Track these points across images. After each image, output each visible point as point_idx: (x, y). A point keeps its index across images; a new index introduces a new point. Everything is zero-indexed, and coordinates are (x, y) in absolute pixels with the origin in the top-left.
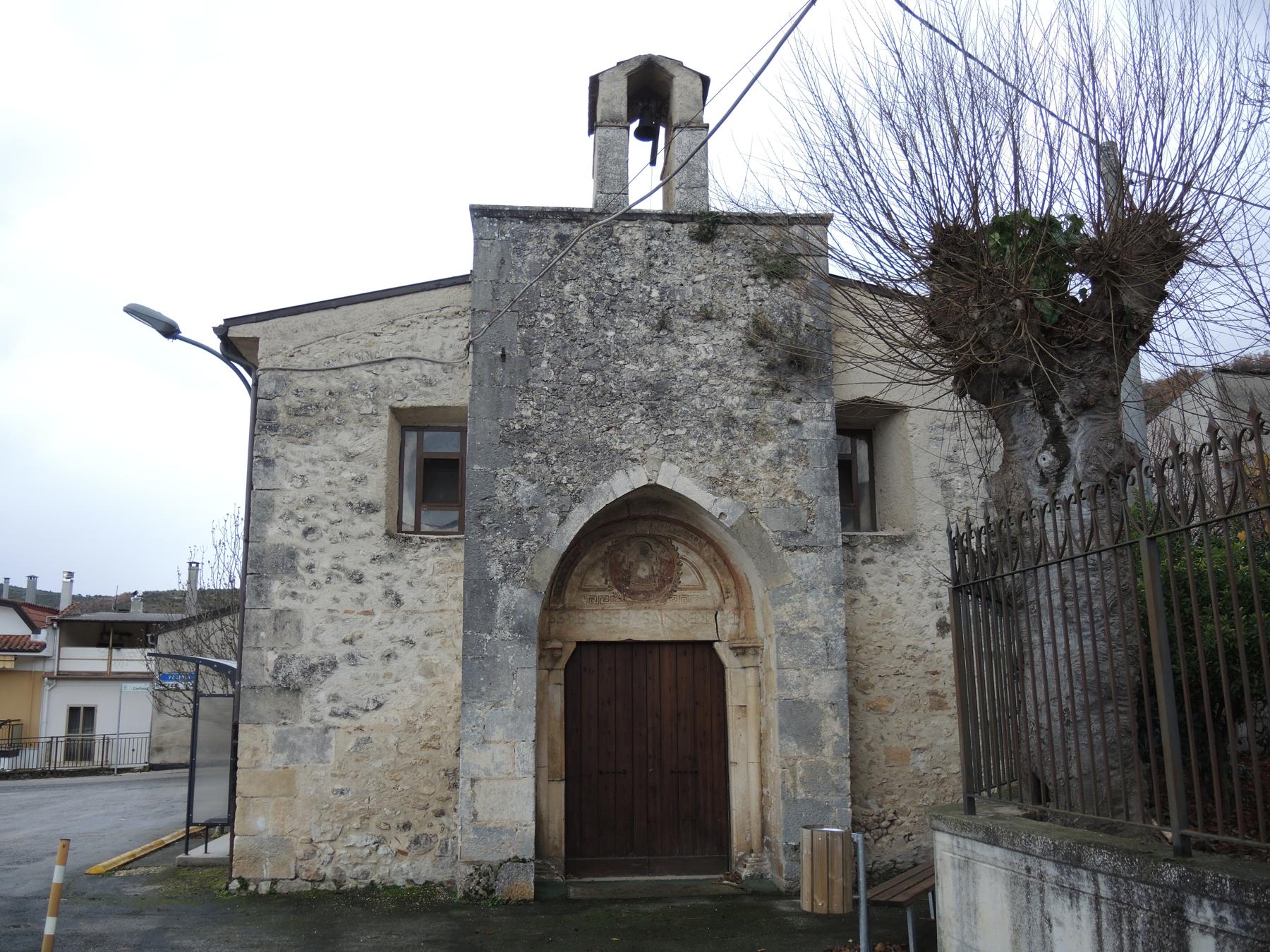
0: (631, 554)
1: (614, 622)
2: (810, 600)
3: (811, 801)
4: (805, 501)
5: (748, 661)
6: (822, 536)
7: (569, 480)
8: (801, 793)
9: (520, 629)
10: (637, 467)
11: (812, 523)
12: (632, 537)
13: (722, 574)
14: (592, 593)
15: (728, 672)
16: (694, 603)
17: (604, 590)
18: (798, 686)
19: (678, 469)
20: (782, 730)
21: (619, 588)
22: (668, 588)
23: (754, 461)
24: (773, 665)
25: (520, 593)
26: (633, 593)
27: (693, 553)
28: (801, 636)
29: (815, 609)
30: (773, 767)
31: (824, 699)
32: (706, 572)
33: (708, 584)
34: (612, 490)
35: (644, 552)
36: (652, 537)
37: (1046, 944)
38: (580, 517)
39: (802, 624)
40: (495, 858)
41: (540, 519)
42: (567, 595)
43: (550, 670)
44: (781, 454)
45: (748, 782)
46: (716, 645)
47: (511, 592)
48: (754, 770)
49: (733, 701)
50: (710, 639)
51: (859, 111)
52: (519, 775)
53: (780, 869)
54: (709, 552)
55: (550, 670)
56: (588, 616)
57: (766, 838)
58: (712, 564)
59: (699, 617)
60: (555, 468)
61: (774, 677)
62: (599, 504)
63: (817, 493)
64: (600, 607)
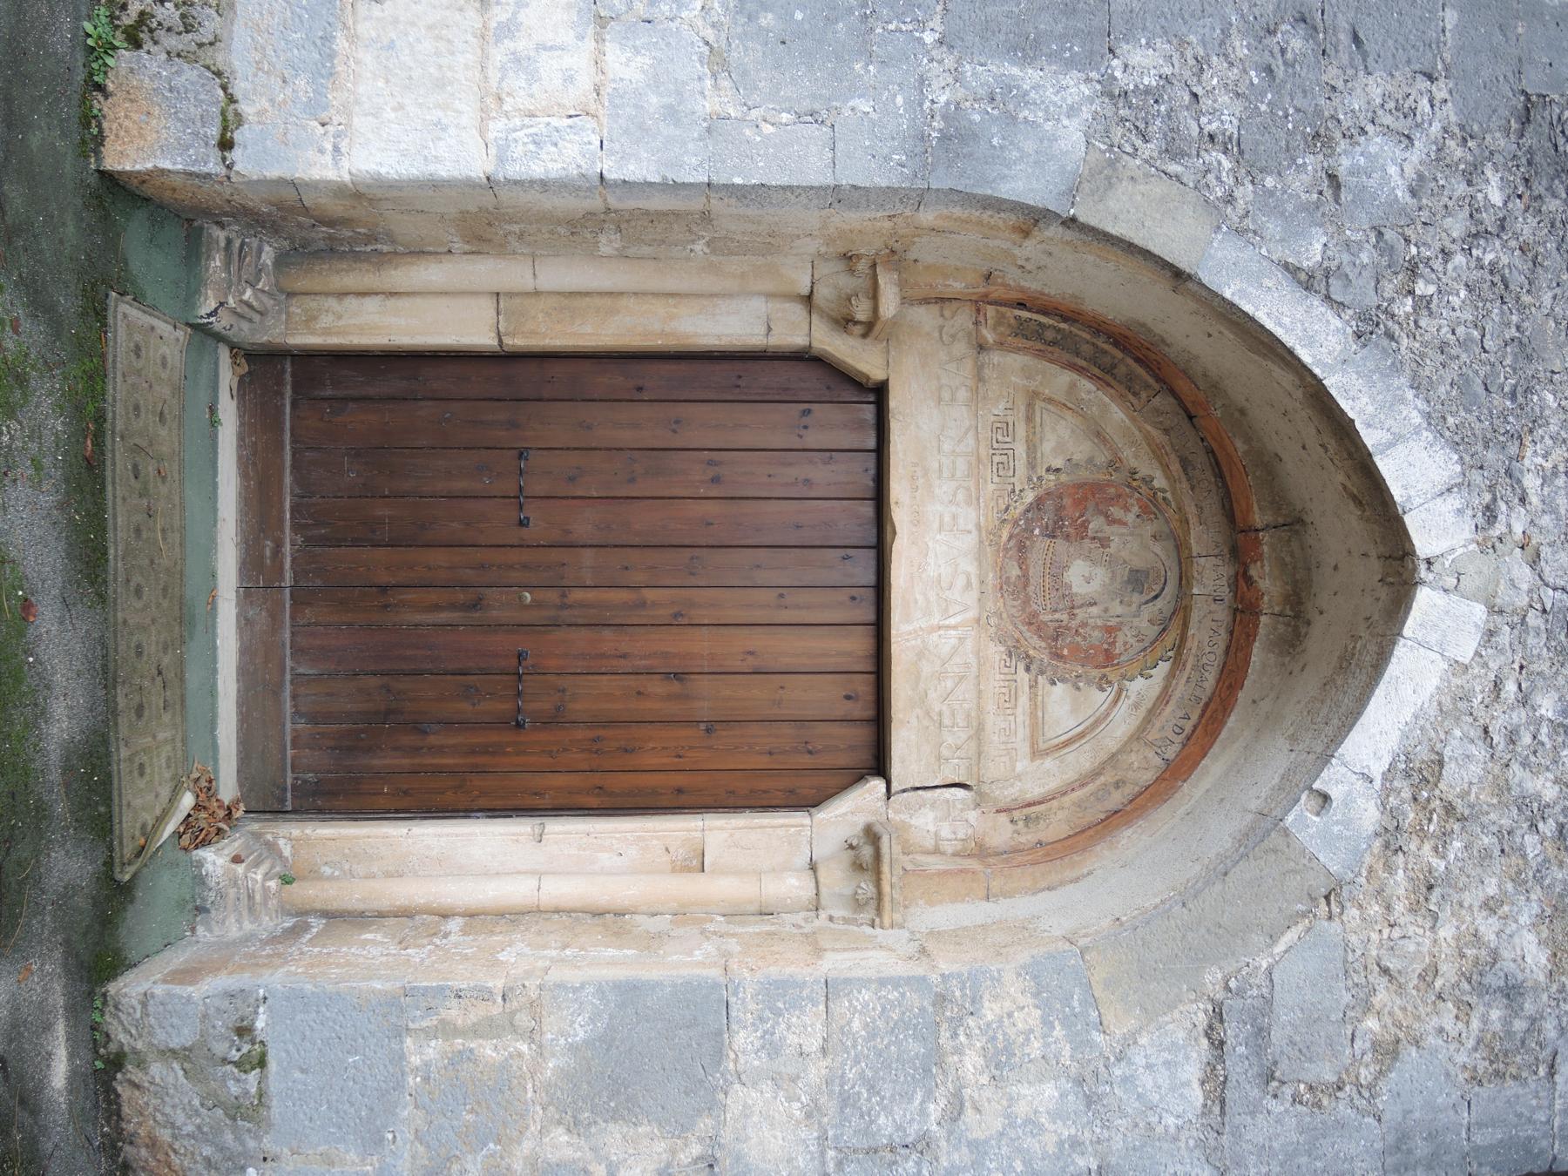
0: (1132, 540)
1: (944, 489)
2: (1050, 1090)
3: (399, 1086)
4: (1365, 1075)
5: (836, 879)
6: (1258, 1130)
7: (1423, 304)
8: (423, 1053)
9: (956, 136)
10: (1467, 531)
11: (1296, 1099)
13: (1079, 804)
14: (1021, 430)
15: (800, 818)
16: (993, 722)
17: (1032, 465)
18: (773, 1048)
19: (1465, 653)
20: (629, 991)
21: (1038, 504)
22: (1036, 646)
23: (1490, 906)
24: (835, 963)
25: (1071, 137)
26: (1022, 548)
28: (933, 1063)
29: (1022, 1109)
30: (518, 957)
31: (727, 1136)
32: (1081, 760)
33: (1049, 763)
34: (1397, 439)
35: (1137, 580)
36: (1182, 610)
38: (1315, 336)
39: (971, 1063)
40: (239, 56)
42: (1015, 361)
43: (808, 300)
44: (1512, 992)
45: (487, 874)
46: (878, 785)
47: (1072, 111)
48: (517, 891)
49: (718, 832)
50: (896, 769)
52: (496, 128)
53: (188, 975)
54: (1143, 767)
55: (808, 300)
56: (960, 415)
57: (317, 924)
58: (1107, 778)
60: (1459, 259)
61: (794, 966)
62: (1355, 397)
63: (1392, 1114)
64: (983, 452)
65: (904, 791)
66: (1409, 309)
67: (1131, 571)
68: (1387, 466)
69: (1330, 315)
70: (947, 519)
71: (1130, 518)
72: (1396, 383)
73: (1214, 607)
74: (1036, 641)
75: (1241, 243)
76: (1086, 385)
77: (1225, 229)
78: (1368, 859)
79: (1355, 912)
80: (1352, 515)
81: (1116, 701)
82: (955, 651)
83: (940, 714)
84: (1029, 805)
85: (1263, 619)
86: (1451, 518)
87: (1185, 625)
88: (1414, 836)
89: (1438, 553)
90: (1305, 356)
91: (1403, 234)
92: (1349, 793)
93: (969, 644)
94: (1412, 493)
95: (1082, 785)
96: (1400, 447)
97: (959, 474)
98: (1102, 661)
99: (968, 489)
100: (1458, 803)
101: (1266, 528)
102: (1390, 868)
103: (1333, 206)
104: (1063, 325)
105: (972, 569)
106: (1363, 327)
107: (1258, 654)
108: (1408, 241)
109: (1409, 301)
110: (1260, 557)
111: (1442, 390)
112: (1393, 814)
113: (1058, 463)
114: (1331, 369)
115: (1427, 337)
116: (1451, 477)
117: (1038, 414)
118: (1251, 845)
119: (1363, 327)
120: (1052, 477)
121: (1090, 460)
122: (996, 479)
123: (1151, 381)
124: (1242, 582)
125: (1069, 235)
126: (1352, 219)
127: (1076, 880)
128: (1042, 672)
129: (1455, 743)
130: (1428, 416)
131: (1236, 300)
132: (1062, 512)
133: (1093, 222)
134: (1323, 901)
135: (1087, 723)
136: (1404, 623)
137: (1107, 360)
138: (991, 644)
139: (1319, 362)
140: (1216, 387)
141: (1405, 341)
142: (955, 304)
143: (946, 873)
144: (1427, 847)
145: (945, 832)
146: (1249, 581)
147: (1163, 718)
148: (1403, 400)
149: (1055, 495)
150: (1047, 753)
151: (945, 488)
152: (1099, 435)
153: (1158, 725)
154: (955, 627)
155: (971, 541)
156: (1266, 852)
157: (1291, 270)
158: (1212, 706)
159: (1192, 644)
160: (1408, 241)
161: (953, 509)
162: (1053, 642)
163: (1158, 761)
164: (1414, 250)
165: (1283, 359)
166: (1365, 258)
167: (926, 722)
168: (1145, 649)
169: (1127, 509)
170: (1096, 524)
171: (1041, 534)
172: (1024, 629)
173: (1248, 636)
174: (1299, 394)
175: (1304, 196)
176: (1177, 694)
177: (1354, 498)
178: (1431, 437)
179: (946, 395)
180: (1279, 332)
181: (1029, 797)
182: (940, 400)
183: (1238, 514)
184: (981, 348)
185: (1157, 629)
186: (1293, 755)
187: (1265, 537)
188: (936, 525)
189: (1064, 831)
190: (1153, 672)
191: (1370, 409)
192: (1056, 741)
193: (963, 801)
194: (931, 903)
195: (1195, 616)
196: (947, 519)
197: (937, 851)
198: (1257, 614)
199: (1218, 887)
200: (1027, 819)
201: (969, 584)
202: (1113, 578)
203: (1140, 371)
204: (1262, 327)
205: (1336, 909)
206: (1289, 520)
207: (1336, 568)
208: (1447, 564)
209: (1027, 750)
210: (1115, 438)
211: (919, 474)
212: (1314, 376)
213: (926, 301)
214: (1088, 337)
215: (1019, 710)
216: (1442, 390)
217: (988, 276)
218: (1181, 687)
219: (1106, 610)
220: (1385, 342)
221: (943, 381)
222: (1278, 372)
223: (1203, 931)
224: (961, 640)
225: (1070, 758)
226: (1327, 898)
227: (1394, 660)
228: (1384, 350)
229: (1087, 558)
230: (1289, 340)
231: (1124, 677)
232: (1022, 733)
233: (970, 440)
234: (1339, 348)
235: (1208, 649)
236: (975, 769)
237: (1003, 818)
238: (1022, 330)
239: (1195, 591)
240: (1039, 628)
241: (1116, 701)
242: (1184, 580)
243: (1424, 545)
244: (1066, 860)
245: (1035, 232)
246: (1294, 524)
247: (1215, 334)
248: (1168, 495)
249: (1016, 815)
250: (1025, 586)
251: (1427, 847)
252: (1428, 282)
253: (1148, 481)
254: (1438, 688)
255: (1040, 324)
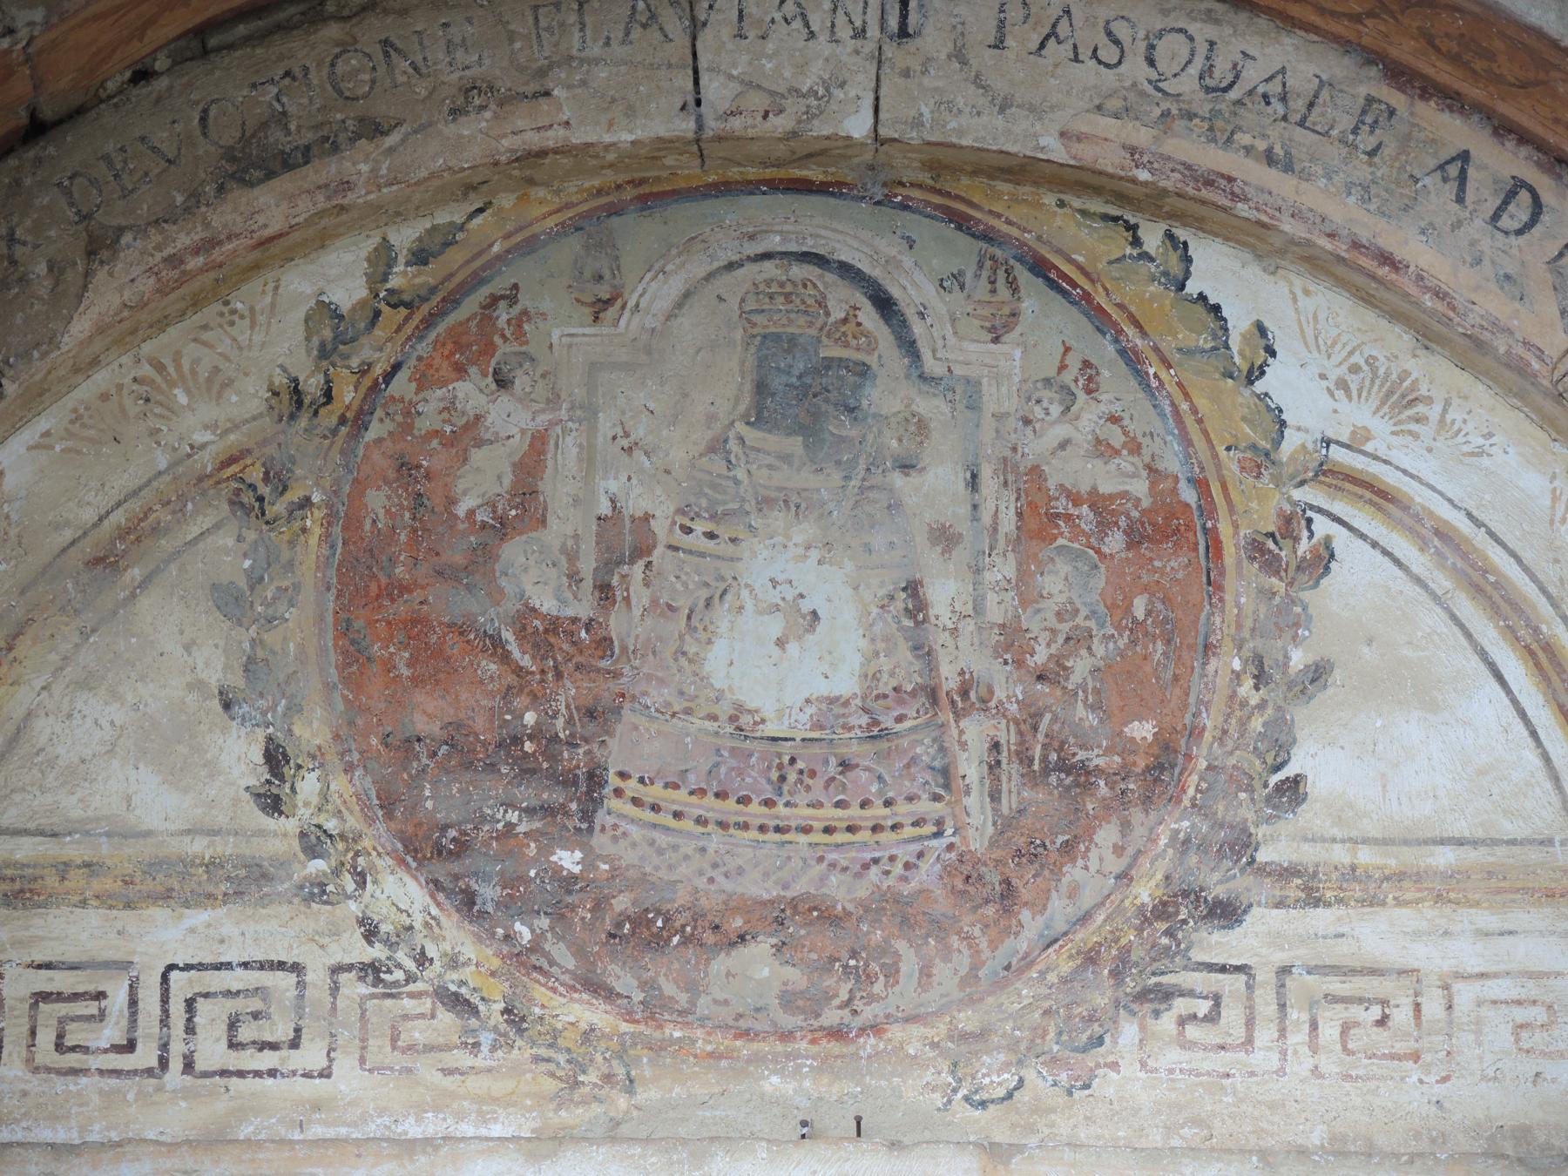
0: (622, 406)
17: (247, 881)
21: (434, 851)
22: (1120, 867)
26: (646, 932)
27: (1476, 407)
36: (946, 187)
37: (4, 36)
51: (1103, 210)
67: (759, 418)
71: (509, 418)
74: (1089, 875)
81: (1379, 496)
87: (1021, 171)
98: (1190, 555)
113: (238, 755)
120: (309, 785)
121: (231, 602)
122: (311, 1055)
128: (1241, 846)
138: (1107, 1085)
149: (396, 771)
153: (1493, 304)
158: (1404, 50)
159: (1108, 144)
168: (1131, 359)
169: (467, 435)
170: (536, 579)
171: (581, 836)
172: (1031, 925)
176: (1349, 214)
185: (1034, 299)
190: (1239, 321)
195: (979, 129)
202: (795, 504)
210: (122, 482)
215: (1427, 956)
218: (1315, 196)
219: (945, 537)
229: (698, 619)
231: (1262, 460)
235: (1136, 69)
239: (858, 126)
240: (1031, 854)
241: (1379, 496)
242: (808, 173)
248: (404, 237)
250: (826, 915)
253: (334, 332)
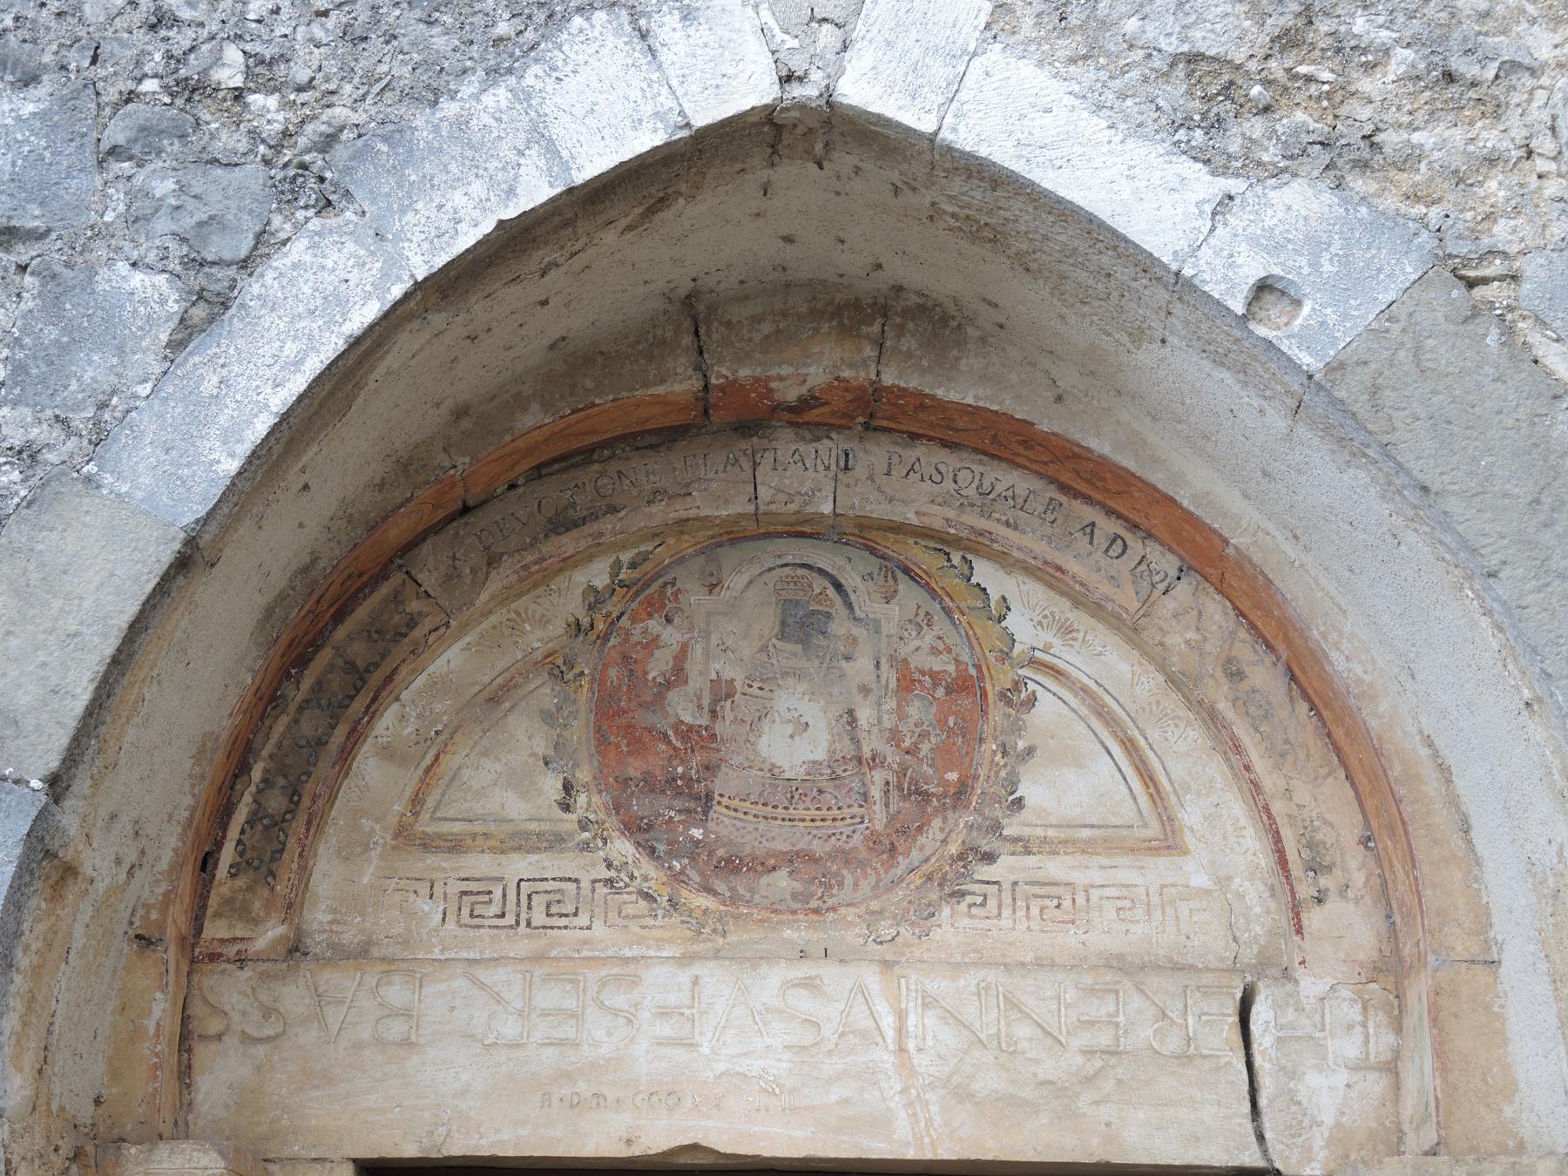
0: (721, 632)
1: (600, 1036)
7: (263, 73)
12: (734, 536)
13: (1280, 754)
14: (479, 864)
16: (1105, 933)
17: (555, 842)
21: (637, 829)
22: (943, 837)
26: (731, 865)
27: (1098, 635)
32: (1182, 749)
33: (1191, 816)
34: (538, 134)
36: (864, 535)
38: (322, 294)
41: (53, 306)
54: (1195, 621)
56: (441, 999)
58: (1221, 696)
59: (1137, 1017)
62: (452, 217)
64: (522, 945)
65: (1260, 1137)
66: (272, 102)
67: (782, 636)
68: (594, 160)
69: (281, 262)
70: (666, 1029)
71: (672, 637)
72: (425, 134)
73: (860, 471)
75: (124, 436)
76: (387, 725)
77: (91, 468)
78: (1390, 202)
79: (1501, 229)
80: (684, 214)
81: (1056, 673)
82: (951, 1017)
83: (1089, 1053)
84: (1283, 862)
85: (888, 379)
86: (700, 34)
87: (899, 528)
88: (1344, 111)
89: (768, 60)
90: (365, 314)
91: (116, 107)
92: (1253, 241)
93: (937, 985)
94: (648, 109)
95: (1237, 748)
96: (555, 131)
97: (571, 1003)
98: (972, 700)
99: (603, 983)
100: (1275, 24)
101: (701, 370)
102: (1409, 159)
103: (51, 244)
104: (257, 773)
105: (774, 977)
106: (309, 195)
107: (962, 391)
108: (130, 97)
109: (256, 100)
110: (761, 383)
111: (440, 42)
112: (1296, 154)
113: (551, 786)
114: (394, 262)
115: (332, 67)
116: (618, 32)
117: (446, 827)
118: (1363, 436)
119: (309, 195)
120: (582, 799)
121: (548, 718)
122: (583, 919)
123: (385, 589)
124: (813, 415)
125: (81, 784)
126: (81, 207)
127: (1444, 771)
128: (996, 828)
129: (1151, 32)
130: (494, 73)
131: (244, 449)
132: (658, 781)
133: (62, 739)
134: (1479, 292)
135: (1105, 734)
136: (909, 130)
137: (336, 681)
138: (936, 934)
139: (379, 288)
140: (407, 465)
141: (340, 113)
142: (197, 1009)
143: (1439, 1054)
144: (1366, 85)
145: (1351, 1048)
146: (808, 402)
147: (1092, 579)
148: (461, 123)
149: (620, 792)
150: (1168, 820)
151: (599, 1034)
152: (496, 698)
153: (1106, 589)
154: (901, 1016)
155: (716, 979)
156: (1377, 408)
157: (184, 336)
158: (1066, 477)
159: (937, 518)
160: (130, 97)
161: (645, 1015)
162: (934, 803)
163: (1183, 589)
164: (150, 85)
165: (368, 353)
166: (164, 187)
167: (1109, 1086)
168: (947, 612)
169: (653, 644)
170: (683, 708)
171: (702, 823)
172: (903, 863)
173: (923, 406)
174: (437, 320)
175: (29, 303)
176: (1041, 548)
177: (651, 211)
178: (536, 69)
179: (397, 1029)
180: (314, 365)
181: (1265, 860)
182: (407, 1043)
183: (667, 422)
184: (295, 949)
185: (904, 585)
186: (1173, 340)
187: (720, 373)
188: (680, 1054)
189: (1336, 790)
191: (478, 188)
192: (1143, 800)
193: (1277, 1007)
194: (1510, 1089)
195: (880, 510)
196: (666, 1029)
197: (1392, 1068)
198: (878, 390)
199: (1453, 505)
200: (1315, 868)
201: (809, 984)
202: (798, 675)
203: (362, 613)
204: (301, 398)
205: (1496, 267)
206: (687, 324)
207: (788, 240)
208: (792, 43)
209: (1162, 862)
210: (502, 664)
211: (566, 1091)
212: (407, 296)
213: (185, 1074)
214: (284, 720)
215: (1078, 877)
216: (440, 42)
217: (144, 941)
218: (1027, 541)
219: (865, 690)
220: (340, 153)
221: (366, 1035)
222: (392, 360)
223: (1546, 537)
224: (928, 1002)
225: (1178, 770)
226: (1471, 284)
227: (983, 152)
228: (357, 156)
229: (755, 725)
230: (331, 346)
231: (1005, 656)
232: (1126, 871)
233: (497, 976)
234: (350, 246)
235: (948, 485)
236: (1208, 978)
237: (1314, 919)
238: (262, 863)
240: (902, 832)
241: (1056, 673)
242: (803, 529)
243: (752, 89)
244: (1401, 791)
245: (67, 855)
246: (694, 314)
247: (305, 478)
248: (626, 557)
249: (1305, 890)
250: (813, 859)
251: (1366, 85)
252: (218, 61)
254: (1040, 64)
255: (250, 823)
